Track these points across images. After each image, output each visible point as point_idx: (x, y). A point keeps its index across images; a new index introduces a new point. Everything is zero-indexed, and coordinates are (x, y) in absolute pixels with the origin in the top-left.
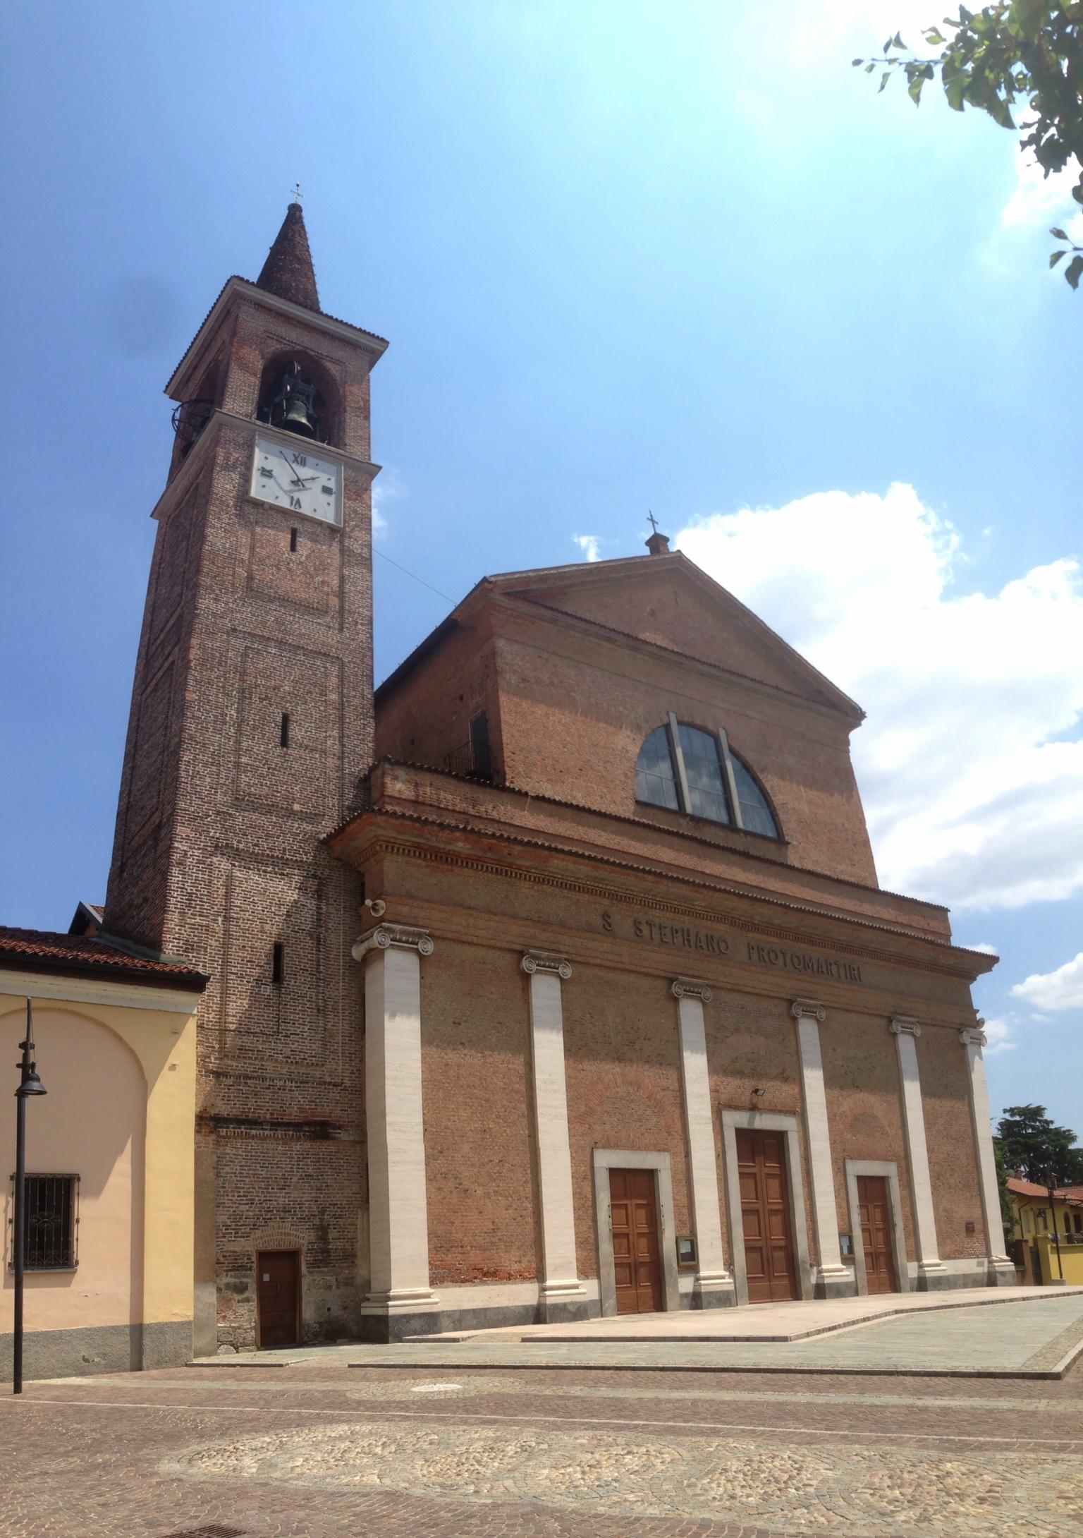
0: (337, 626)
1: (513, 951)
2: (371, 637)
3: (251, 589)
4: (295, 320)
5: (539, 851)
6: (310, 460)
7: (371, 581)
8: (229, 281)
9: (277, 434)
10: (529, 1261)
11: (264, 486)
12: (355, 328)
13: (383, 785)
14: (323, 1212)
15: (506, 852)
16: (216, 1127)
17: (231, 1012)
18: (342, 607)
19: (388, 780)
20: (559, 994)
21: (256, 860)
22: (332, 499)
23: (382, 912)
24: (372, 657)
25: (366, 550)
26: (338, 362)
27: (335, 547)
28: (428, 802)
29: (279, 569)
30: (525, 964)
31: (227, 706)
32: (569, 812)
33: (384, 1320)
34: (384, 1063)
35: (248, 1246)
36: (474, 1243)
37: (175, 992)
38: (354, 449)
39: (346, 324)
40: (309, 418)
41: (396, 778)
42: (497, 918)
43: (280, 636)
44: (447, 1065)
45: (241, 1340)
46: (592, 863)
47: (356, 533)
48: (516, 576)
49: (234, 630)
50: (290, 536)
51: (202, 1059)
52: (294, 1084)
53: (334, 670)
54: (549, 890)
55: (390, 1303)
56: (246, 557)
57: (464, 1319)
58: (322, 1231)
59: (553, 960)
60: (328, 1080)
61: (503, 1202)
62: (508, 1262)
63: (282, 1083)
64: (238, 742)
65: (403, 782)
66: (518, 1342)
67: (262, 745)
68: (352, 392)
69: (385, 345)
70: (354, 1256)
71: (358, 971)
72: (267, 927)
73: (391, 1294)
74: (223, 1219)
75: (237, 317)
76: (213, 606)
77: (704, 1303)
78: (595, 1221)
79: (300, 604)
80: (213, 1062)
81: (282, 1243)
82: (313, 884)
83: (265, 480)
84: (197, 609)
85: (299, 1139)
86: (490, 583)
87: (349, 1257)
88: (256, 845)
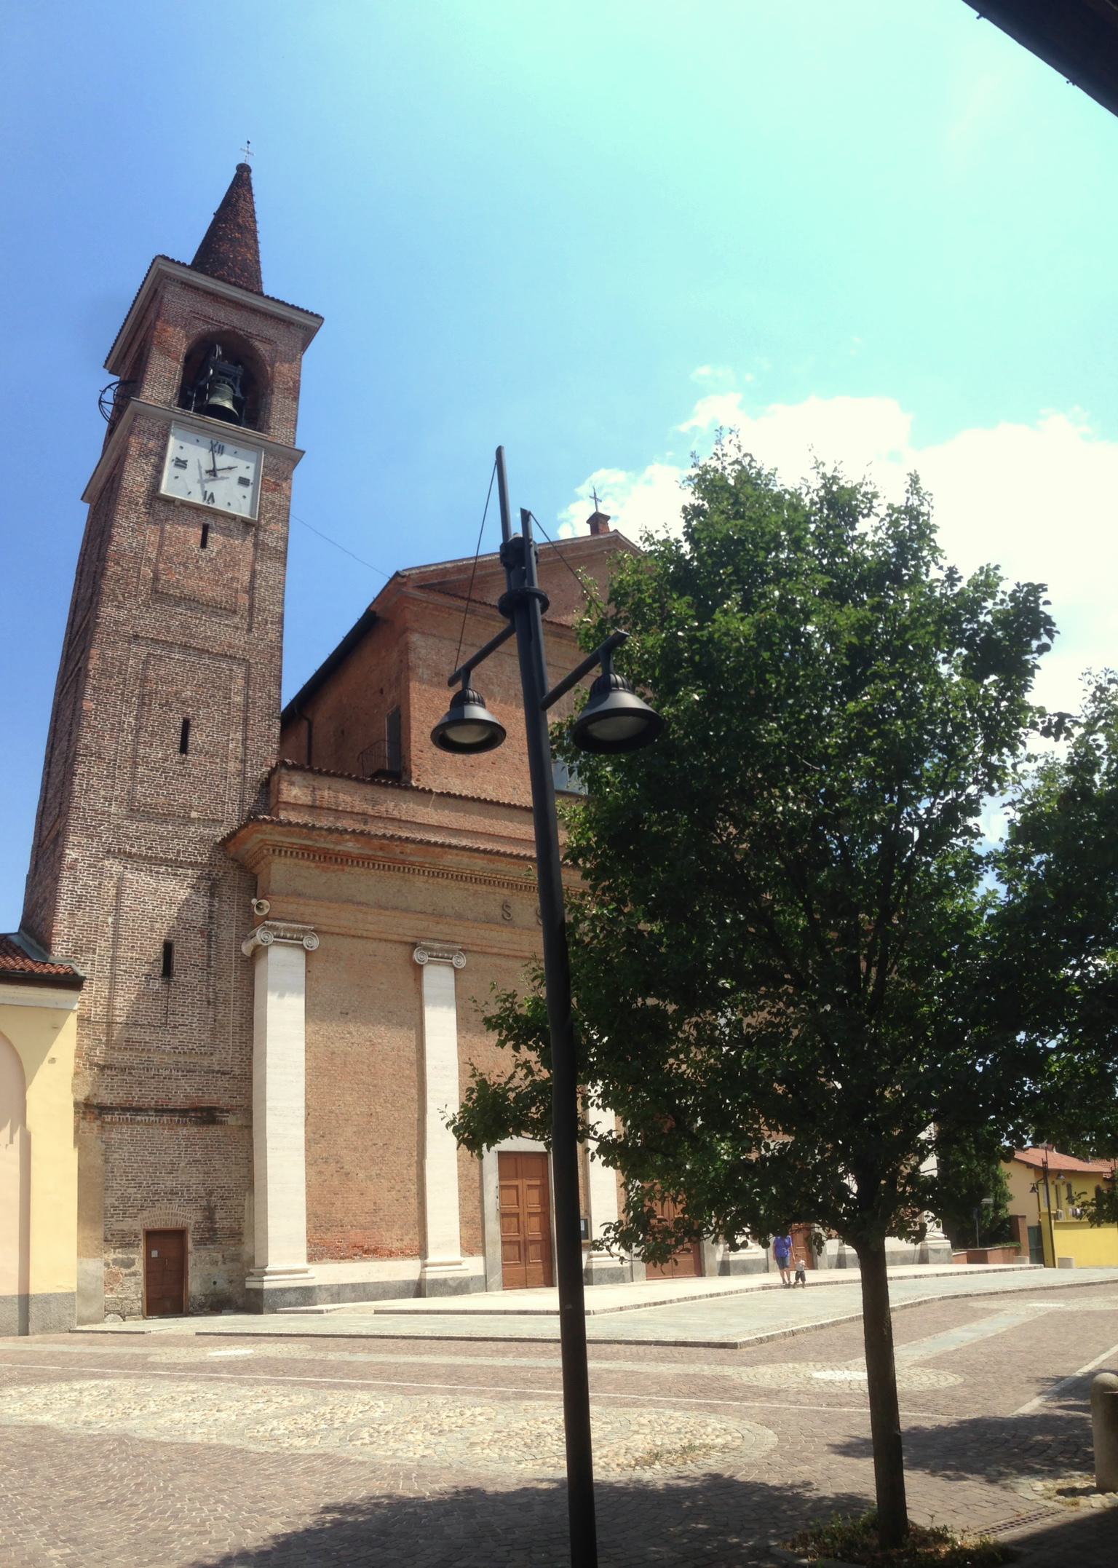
0: (245, 626)
1: (406, 943)
2: (282, 636)
3: (158, 595)
4: (224, 298)
5: (432, 849)
6: (229, 448)
7: (284, 575)
8: (154, 260)
9: (195, 422)
10: (411, 1238)
11: (177, 477)
12: (287, 305)
13: (279, 791)
14: (210, 1194)
15: (398, 850)
16: (100, 1114)
17: (118, 1005)
18: (252, 606)
19: (284, 786)
20: (452, 983)
21: (150, 861)
22: (248, 491)
23: (266, 911)
24: (281, 657)
25: (281, 543)
26: (267, 341)
27: (250, 540)
28: (325, 806)
29: (187, 567)
30: (417, 956)
31: (125, 714)
32: (476, 806)
33: (259, 1292)
34: (265, 1053)
35: (137, 1225)
36: (355, 1223)
37: (54, 990)
38: (278, 433)
39: (278, 301)
40: (235, 401)
41: (292, 784)
42: (387, 913)
43: (184, 640)
44: (333, 1053)
45: (128, 1310)
46: (489, 856)
47: (272, 526)
48: (432, 568)
49: (136, 637)
50: (200, 532)
51: (82, 1053)
52: (180, 1073)
53: (240, 671)
54: (445, 882)
55: (265, 1278)
56: (153, 555)
57: (339, 1293)
58: (209, 1212)
59: (447, 951)
60: (217, 1068)
61: (386, 1184)
62: (389, 1240)
63: (167, 1072)
64: (135, 750)
65: (299, 787)
66: (371, 1314)
67: (161, 750)
68: (283, 368)
69: (319, 321)
70: (241, 1234)
71: (250, 963)
72: (157, 925)
73: (267, 1269)
74: (109, 1201)
75: (162, 297)
76: (114, 612)
77: (595, 1279)
78: (482, 1201)
79: (208, 605)
80: (99, 1055)
81: (169, 1222)
82: (205, 884)
83: (179, 471)
84: (98, 618)
85: (185, 1124)
86: (403, 577)
87: (237, 1235)
88: (150, 848)
